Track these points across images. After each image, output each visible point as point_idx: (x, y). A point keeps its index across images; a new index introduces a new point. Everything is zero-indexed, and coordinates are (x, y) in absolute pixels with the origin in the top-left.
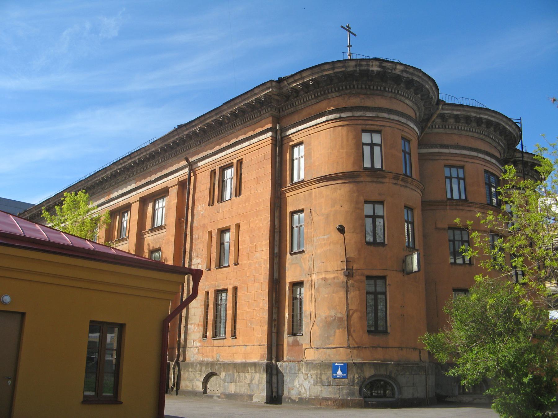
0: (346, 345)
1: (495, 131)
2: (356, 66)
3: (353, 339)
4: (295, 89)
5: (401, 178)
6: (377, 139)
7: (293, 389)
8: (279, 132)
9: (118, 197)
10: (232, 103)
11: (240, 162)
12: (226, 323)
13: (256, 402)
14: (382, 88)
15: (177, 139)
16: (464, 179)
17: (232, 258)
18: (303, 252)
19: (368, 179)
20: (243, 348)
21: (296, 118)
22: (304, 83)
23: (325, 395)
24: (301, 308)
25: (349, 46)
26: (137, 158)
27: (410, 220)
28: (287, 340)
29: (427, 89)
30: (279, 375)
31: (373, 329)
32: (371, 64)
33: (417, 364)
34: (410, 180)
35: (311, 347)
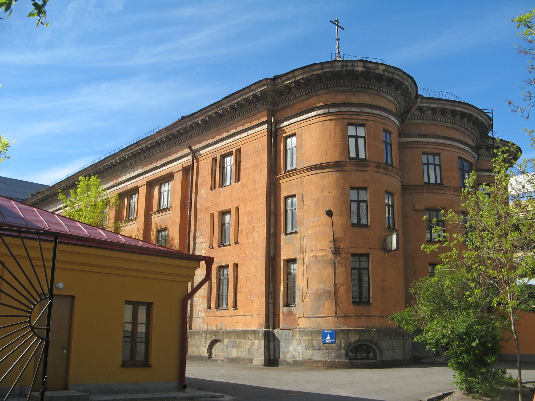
0: (334, 315)
1: (468, 122)
2: (342, 66)
3: (340, 309)
4: (289, 86)
5: (382, 167)
6: (361, 131)
7: (288, 353)
8: (274, 125)
9: (127, 180)
10: (231, 98)
11: (239, 151)
12: (228, 295)
13: (256, 365)
14: (366, 86)
15: (181, 129)
16: (439, 165)
17: (232, 238)
18: (296, 232)
19: (353, 168)
20: (244, 318)
21: (289, 112)
22: (296, 81)
23: (316, 357)
24: (294, 282)
25: (338, 40)
26: (144, 145)
27: (390, 203)
28: (282, 310)
29: (406, 86)
30: (276, 341)
31: (357, 300)
32: (356, 64)
33: (397, 330)
34: (390, 168)
35: (304, 317)
